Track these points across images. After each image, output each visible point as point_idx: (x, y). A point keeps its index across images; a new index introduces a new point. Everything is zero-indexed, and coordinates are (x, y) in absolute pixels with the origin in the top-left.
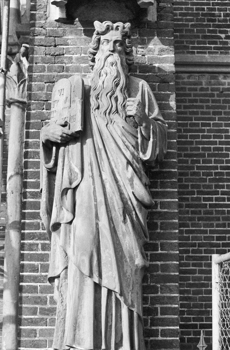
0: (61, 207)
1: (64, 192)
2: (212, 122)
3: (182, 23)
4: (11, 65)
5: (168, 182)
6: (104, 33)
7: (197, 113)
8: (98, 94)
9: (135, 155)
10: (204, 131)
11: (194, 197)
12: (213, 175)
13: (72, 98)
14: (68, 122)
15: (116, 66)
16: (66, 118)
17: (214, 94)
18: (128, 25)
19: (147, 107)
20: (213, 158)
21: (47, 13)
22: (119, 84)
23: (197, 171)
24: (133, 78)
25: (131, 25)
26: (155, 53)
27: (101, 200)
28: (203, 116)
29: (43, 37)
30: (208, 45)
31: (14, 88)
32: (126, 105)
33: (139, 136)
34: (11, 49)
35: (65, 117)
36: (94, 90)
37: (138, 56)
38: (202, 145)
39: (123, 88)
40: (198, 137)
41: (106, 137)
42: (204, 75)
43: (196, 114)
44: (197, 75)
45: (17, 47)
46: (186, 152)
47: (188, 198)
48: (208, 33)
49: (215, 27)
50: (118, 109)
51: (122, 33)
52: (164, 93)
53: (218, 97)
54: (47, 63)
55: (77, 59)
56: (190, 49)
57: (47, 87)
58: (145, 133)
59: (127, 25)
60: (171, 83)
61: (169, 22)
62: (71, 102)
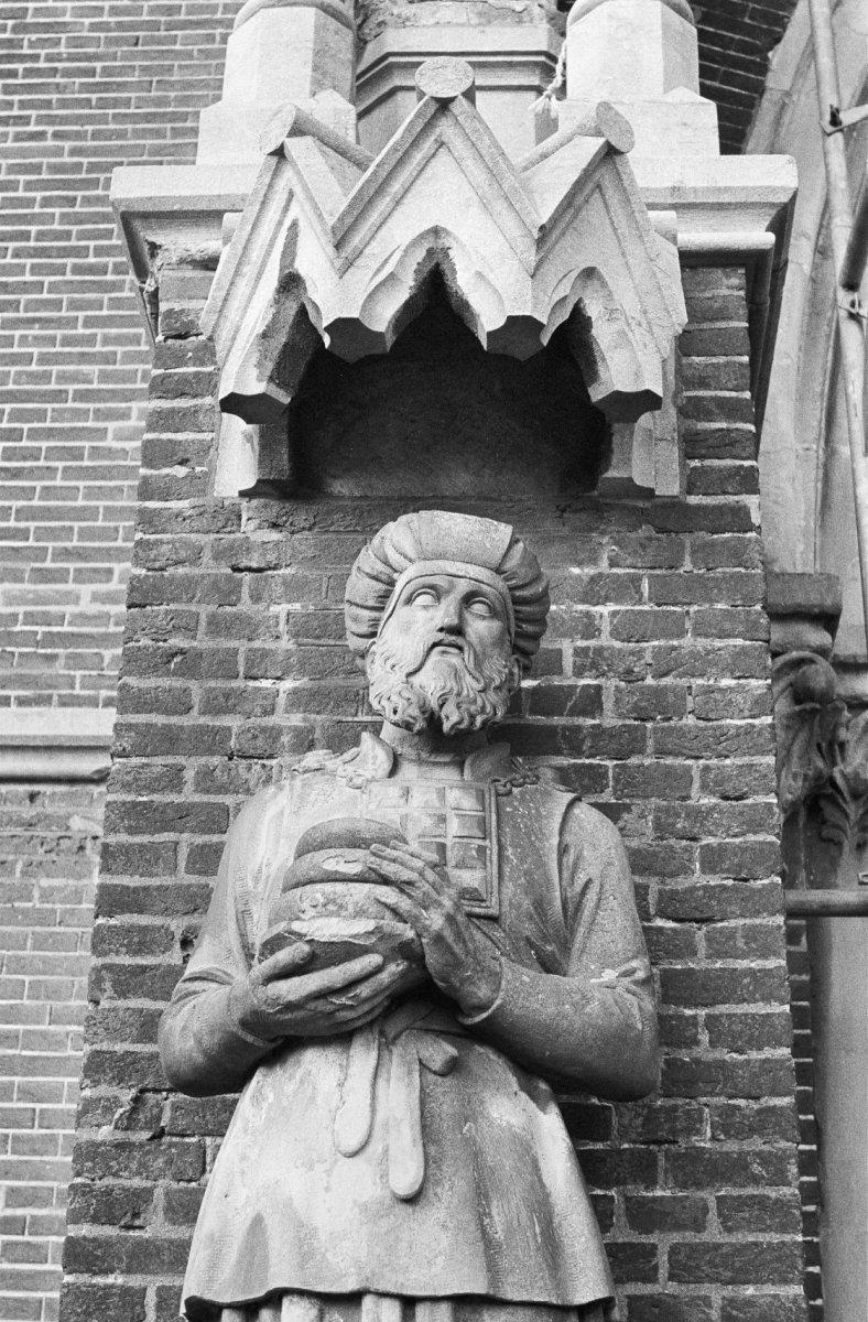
28: (23, 228)
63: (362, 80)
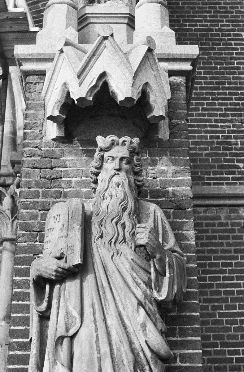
0: (55, 360)
1: (59, 340)
2: (234, 262)
3: (195, 152)
4: (4, 197)
5: (189, 328)
6: (107, 149)
7: (216, 251)
8: (102, 220)
9: (147, 294)
10: (224, 272)
11: (217, 350)
12: (239, 323)
13: (69, 225)
14: (64, 253)
15: (122, 187)
16: (62, 249)
17: (235, 229)
18: (136, 140)
19: (161, 236)
20: (237, 303)
21: (43, 132)
22: (127, 208)
23: (220, 318)
24: (143, 202)
25: (140, 141)
26: (168, 175)
27: (106, 351)
28: (223, 255)
29: (38, 158)
30: (225, 176)
31: (7, 224)
32: (135, 233)
33: (152, 270)
34: (5, 180)
35: (61, 248)
36: (96, 216)
37: (149, 178)
38: (224, 288)
39: (132, 213)
40: (218, 279)
41: (111, 272)
42: (222, 209)
43: (215, 253)
44: (215, 208)
45: (12, 178)
46: (205, 297)
47: (210, 351)
48: (224, 163)
49: (232, 156)
50: (126, 238)
51: (129, 148)
52: (180, 221)
53: (239, 233)
54: (42, 188)
55: (77, 183)
56: (205, 180)
57: (42, 215)
58: (159, 266)
59: (135, 140)
60: (188, 210)
61: (184, 140)
62: (68, 230)
63: (80, 20)
